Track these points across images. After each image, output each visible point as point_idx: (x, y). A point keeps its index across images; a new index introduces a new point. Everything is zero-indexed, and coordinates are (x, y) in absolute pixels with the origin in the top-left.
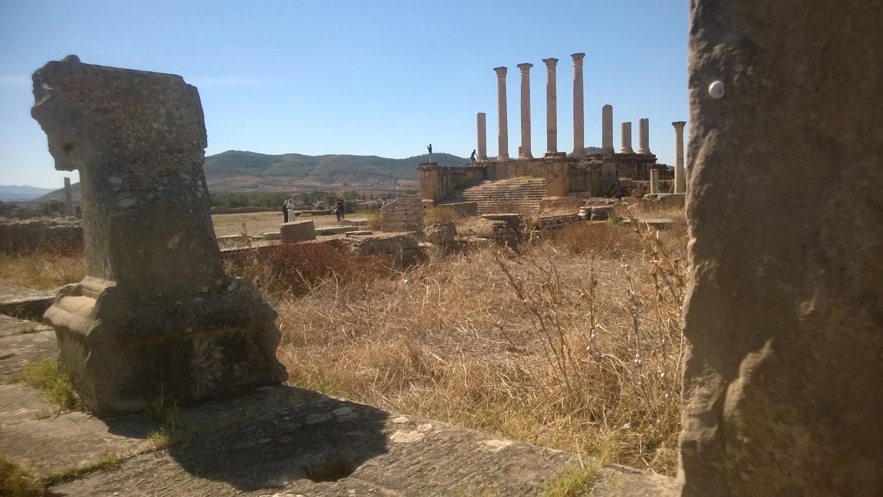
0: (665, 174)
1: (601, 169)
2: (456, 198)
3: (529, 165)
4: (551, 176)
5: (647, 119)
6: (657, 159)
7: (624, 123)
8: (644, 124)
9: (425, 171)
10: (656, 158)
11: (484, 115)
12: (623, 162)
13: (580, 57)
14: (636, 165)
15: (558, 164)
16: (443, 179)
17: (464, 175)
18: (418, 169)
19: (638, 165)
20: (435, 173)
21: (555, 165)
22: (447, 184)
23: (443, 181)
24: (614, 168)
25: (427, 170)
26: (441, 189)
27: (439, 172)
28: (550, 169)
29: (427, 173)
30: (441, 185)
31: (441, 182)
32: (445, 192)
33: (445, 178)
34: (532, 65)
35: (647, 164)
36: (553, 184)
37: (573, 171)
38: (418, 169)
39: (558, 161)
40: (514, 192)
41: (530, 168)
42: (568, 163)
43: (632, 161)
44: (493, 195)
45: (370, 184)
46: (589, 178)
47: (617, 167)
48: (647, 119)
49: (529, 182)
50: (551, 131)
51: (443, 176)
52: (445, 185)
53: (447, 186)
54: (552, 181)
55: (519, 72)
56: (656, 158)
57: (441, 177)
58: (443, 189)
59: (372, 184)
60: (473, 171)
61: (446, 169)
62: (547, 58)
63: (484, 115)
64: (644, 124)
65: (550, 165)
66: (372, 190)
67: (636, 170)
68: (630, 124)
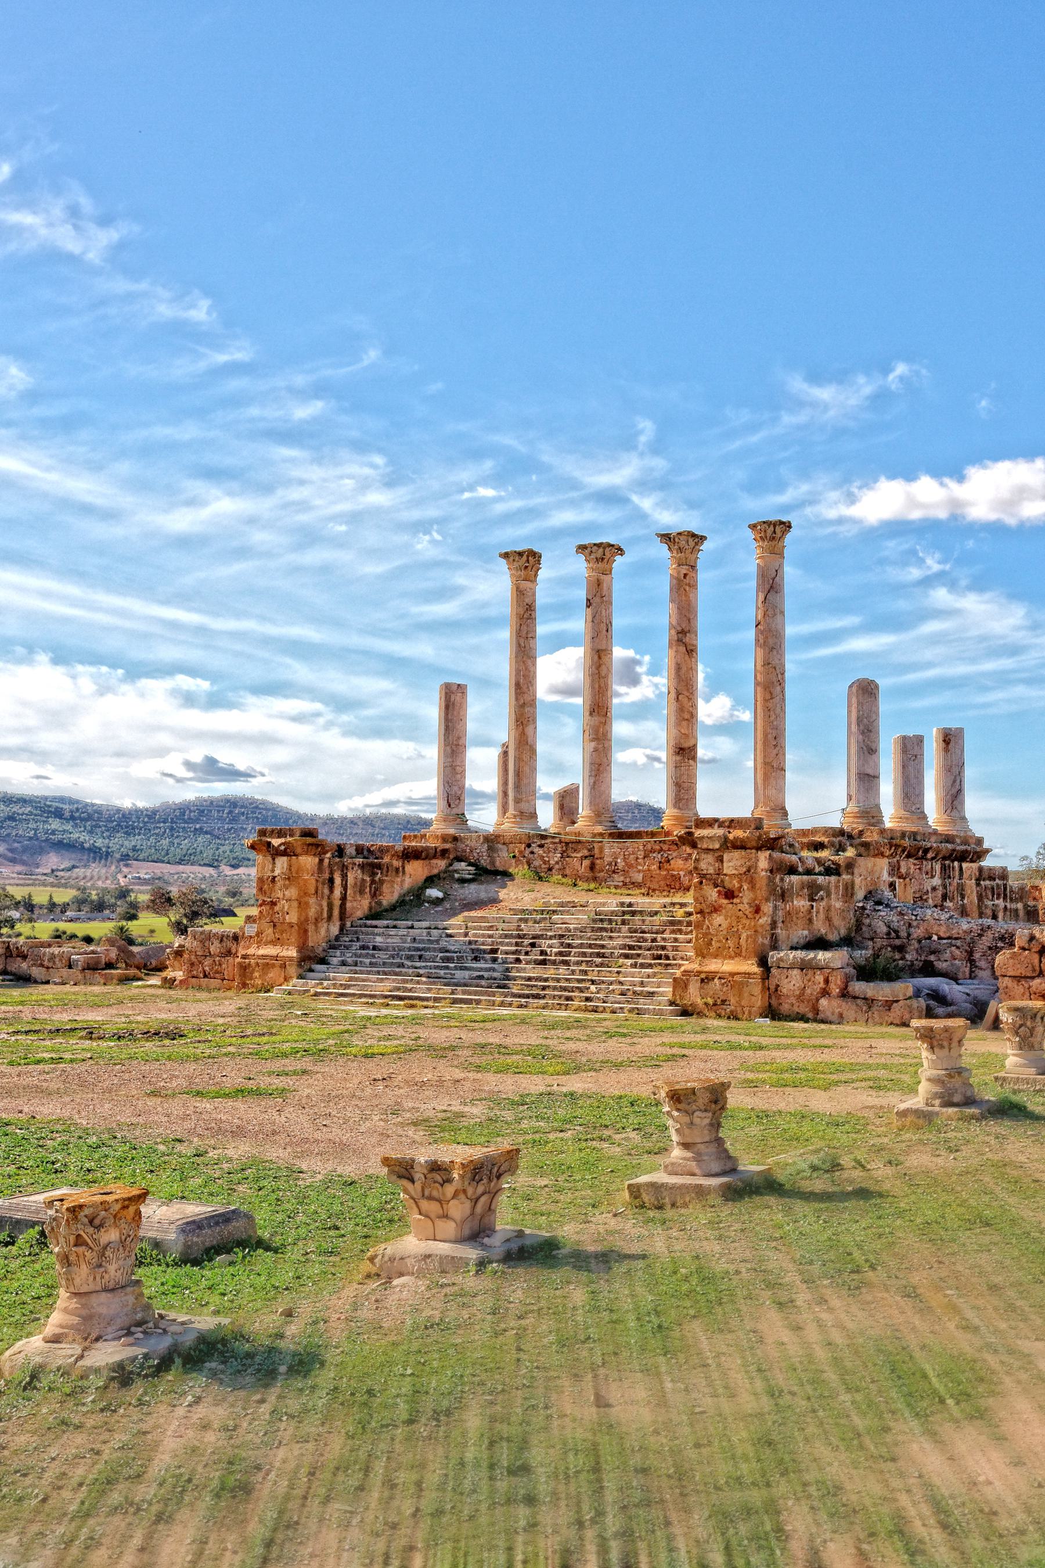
0: (1005, 898)
1: (853, 874)
2: (375, 948)
3: (607, 851)
4: (712, 894)
5: (961, 730)
6: (987, 851)
7: (904, 738)
8: (950, 740)
9: (275, 853)
10: (986, 845)
11: (461, 689)
12: (908, 856)
13: (779, 534)
14: (938, 867)
15: (737, 854)
16: (331, 881)
17: (397, 870)
18: (253, 847)
19: (944, 868)
20: (308, 861)
21: (726, 857)
22: (344, 898)
23: (331, 889)
24: (885, 876)
25: (284, 853)
26: (325, 915)
27: (321, 861)
28: (711, 871)
29: (282, 862)
30: (325, 904)
31: (326, 891)
32: (338, 924)
33: (338, 881)
34: (620, 551)
35: (965, 865)
36: (718, 919)
37: (782, 880)
38: (253, 847)
39: (739, 845)
40: (573, 938)
41: (608, 859)
42: (769, 852)
43: (930, 855)
44: (502, 944)
45: (49, 871)
46: (823, 904)
47: (895, 870)
48: (961, 730)
49: (622, 904)
50: (681, 749)
51: (332, 873)
52: (337, 903)
53: (343, 906)
54: (716, 909)
55: (580, 567)
56: (986, 845)
57: (327, 876)
58: (330, 917)
59: (53, 871)
60: (427, 862)
61: (340, 850)
62: (674, 531)
63: (461, 689)
64: (950, 740)
65: (710, 858)
66: (53, 885)
67: (937, 881)
68: (919, 740)
